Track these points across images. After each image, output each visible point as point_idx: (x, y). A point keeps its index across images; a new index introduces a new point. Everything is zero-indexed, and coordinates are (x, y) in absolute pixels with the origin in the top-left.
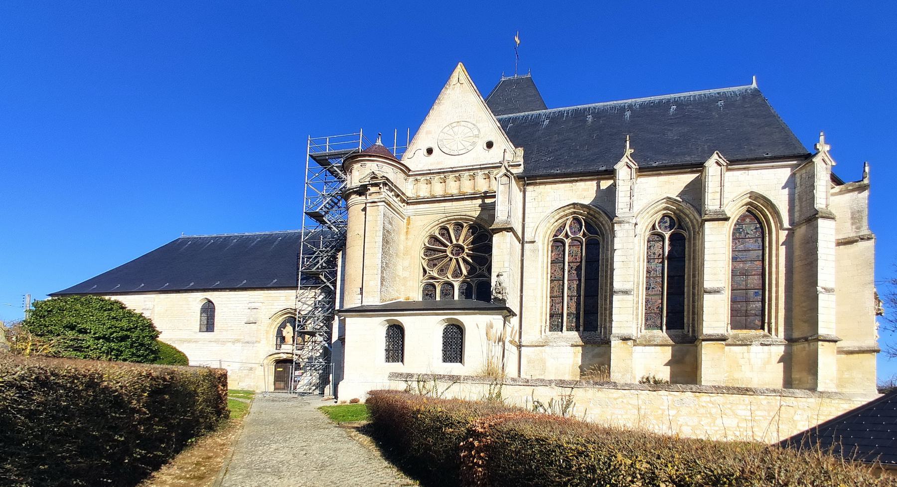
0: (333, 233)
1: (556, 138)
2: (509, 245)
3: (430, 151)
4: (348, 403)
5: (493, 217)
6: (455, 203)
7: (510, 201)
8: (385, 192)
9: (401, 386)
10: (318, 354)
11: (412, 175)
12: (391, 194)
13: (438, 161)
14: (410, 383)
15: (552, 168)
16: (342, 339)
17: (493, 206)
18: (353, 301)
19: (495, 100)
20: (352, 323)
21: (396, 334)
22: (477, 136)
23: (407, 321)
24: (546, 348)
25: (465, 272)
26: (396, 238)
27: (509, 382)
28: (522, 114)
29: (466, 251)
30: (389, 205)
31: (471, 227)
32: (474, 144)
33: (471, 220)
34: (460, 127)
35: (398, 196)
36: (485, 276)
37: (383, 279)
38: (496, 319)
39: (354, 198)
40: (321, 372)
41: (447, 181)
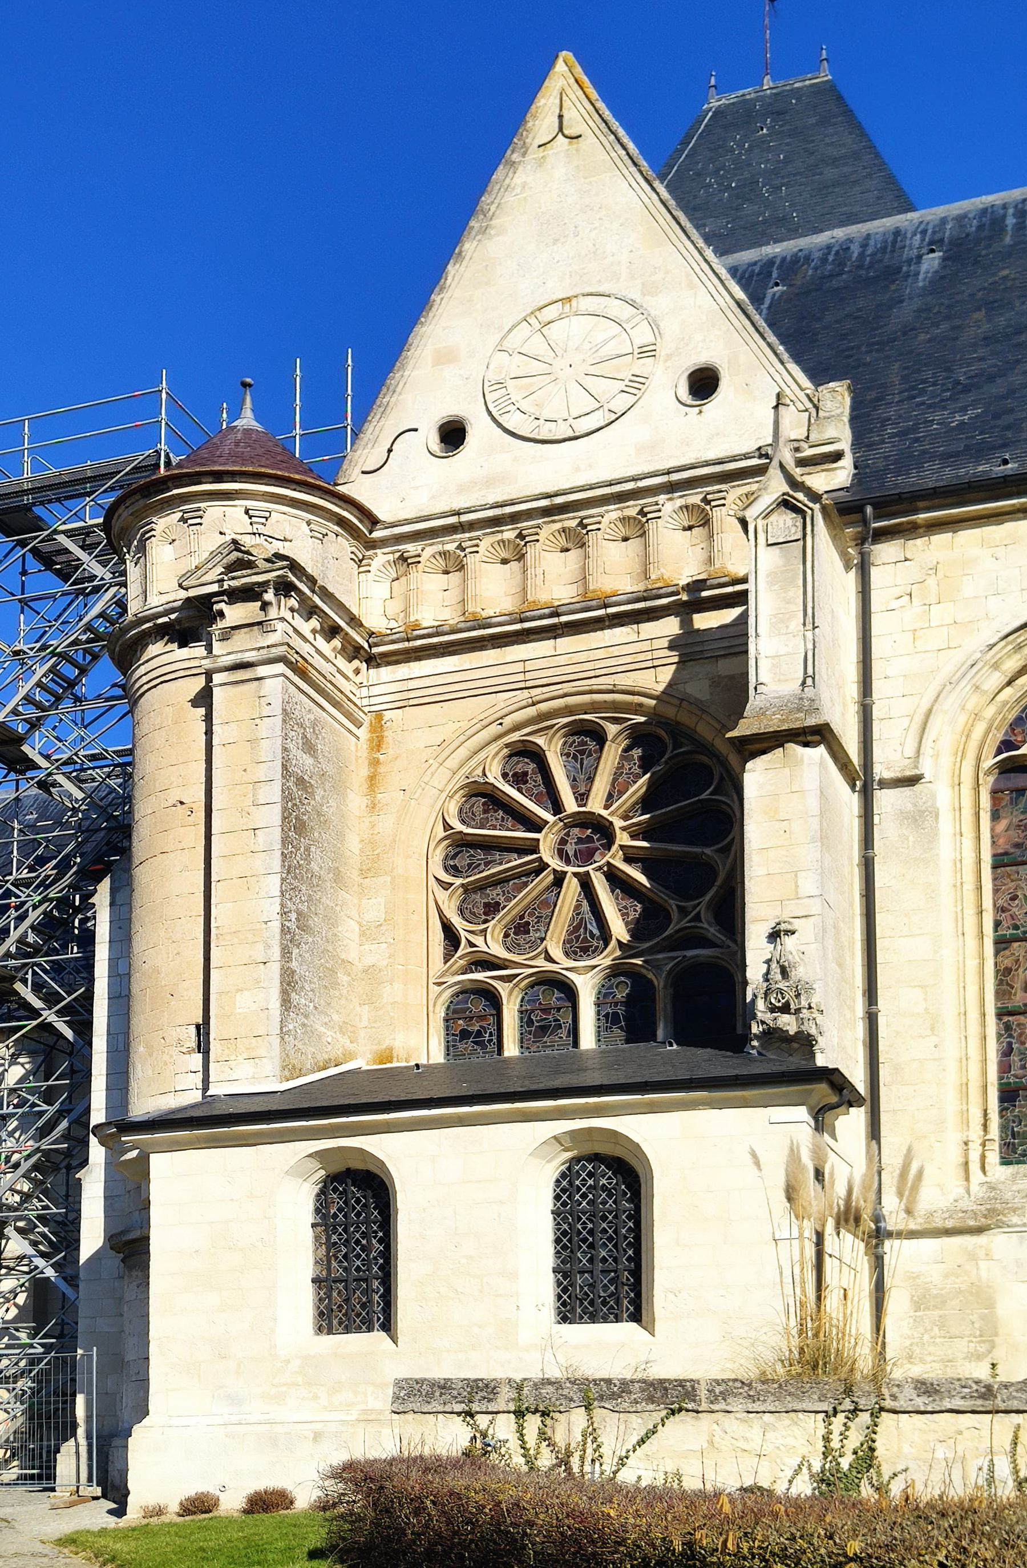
0: (54, 813)
1: (978, 324)
2: (813, 803)
3: (453, 435)
4: (172, 1514)
5: (736, 690)
6: (566, 643)
7: (810, 621)
8: (287, 624)
9: (448, 1436)
10: (14, 1312)
11: (383, 542)
12: (306, 627)
13: (496, 471)
14: (483, 1421)
15: (980, 452)
16: (130, 1246)
17: (735, 641)
18: (166, 1083)
19: (711, 183)
20: (182, 1181)
21: (358, 1211)
22: (647, 352)
23: (403, 1153)
24: (996, 1241)
25: (619, 930)
26: (330, 809)
27: (907, 1398)
28: (823, 238)
29: (623, 839)
30: (303, 674)
31: (637, 737)
32: (637, 384)
33: (638, 709)
34: (582, 325)
35: (332, 631)
36: (704, 942)
37: (289, 982)
38: (791, 1121)
39: (161, 655)
40: (24, 1384)
41: (531, 551)
